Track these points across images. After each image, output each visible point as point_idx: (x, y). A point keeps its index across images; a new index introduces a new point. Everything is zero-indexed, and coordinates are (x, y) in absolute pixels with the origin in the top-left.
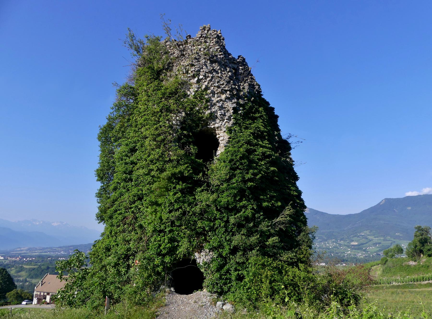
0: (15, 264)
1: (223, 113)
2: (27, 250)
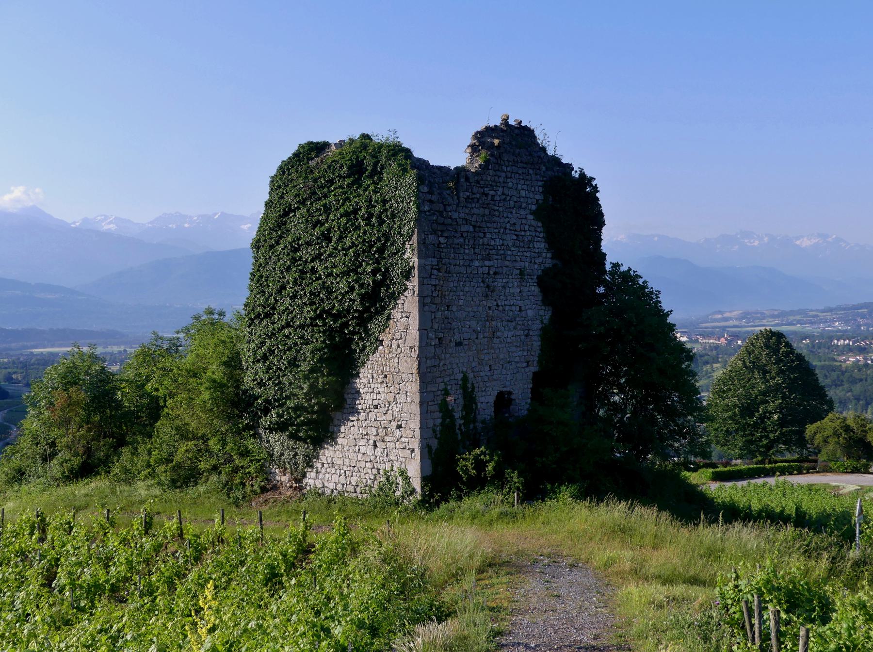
2: (740, 318)
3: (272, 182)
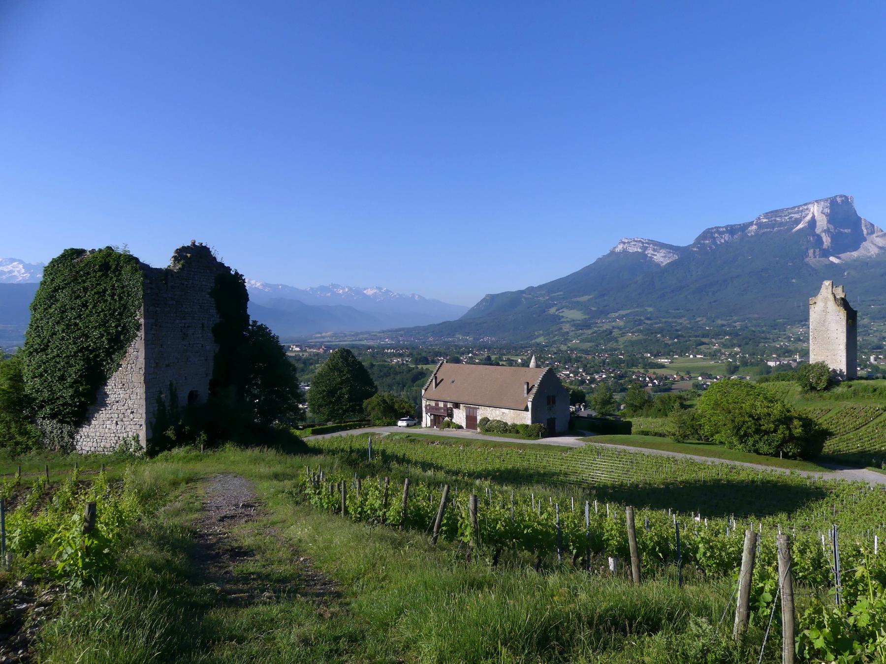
2: (331, 337)
3: (45, 270)
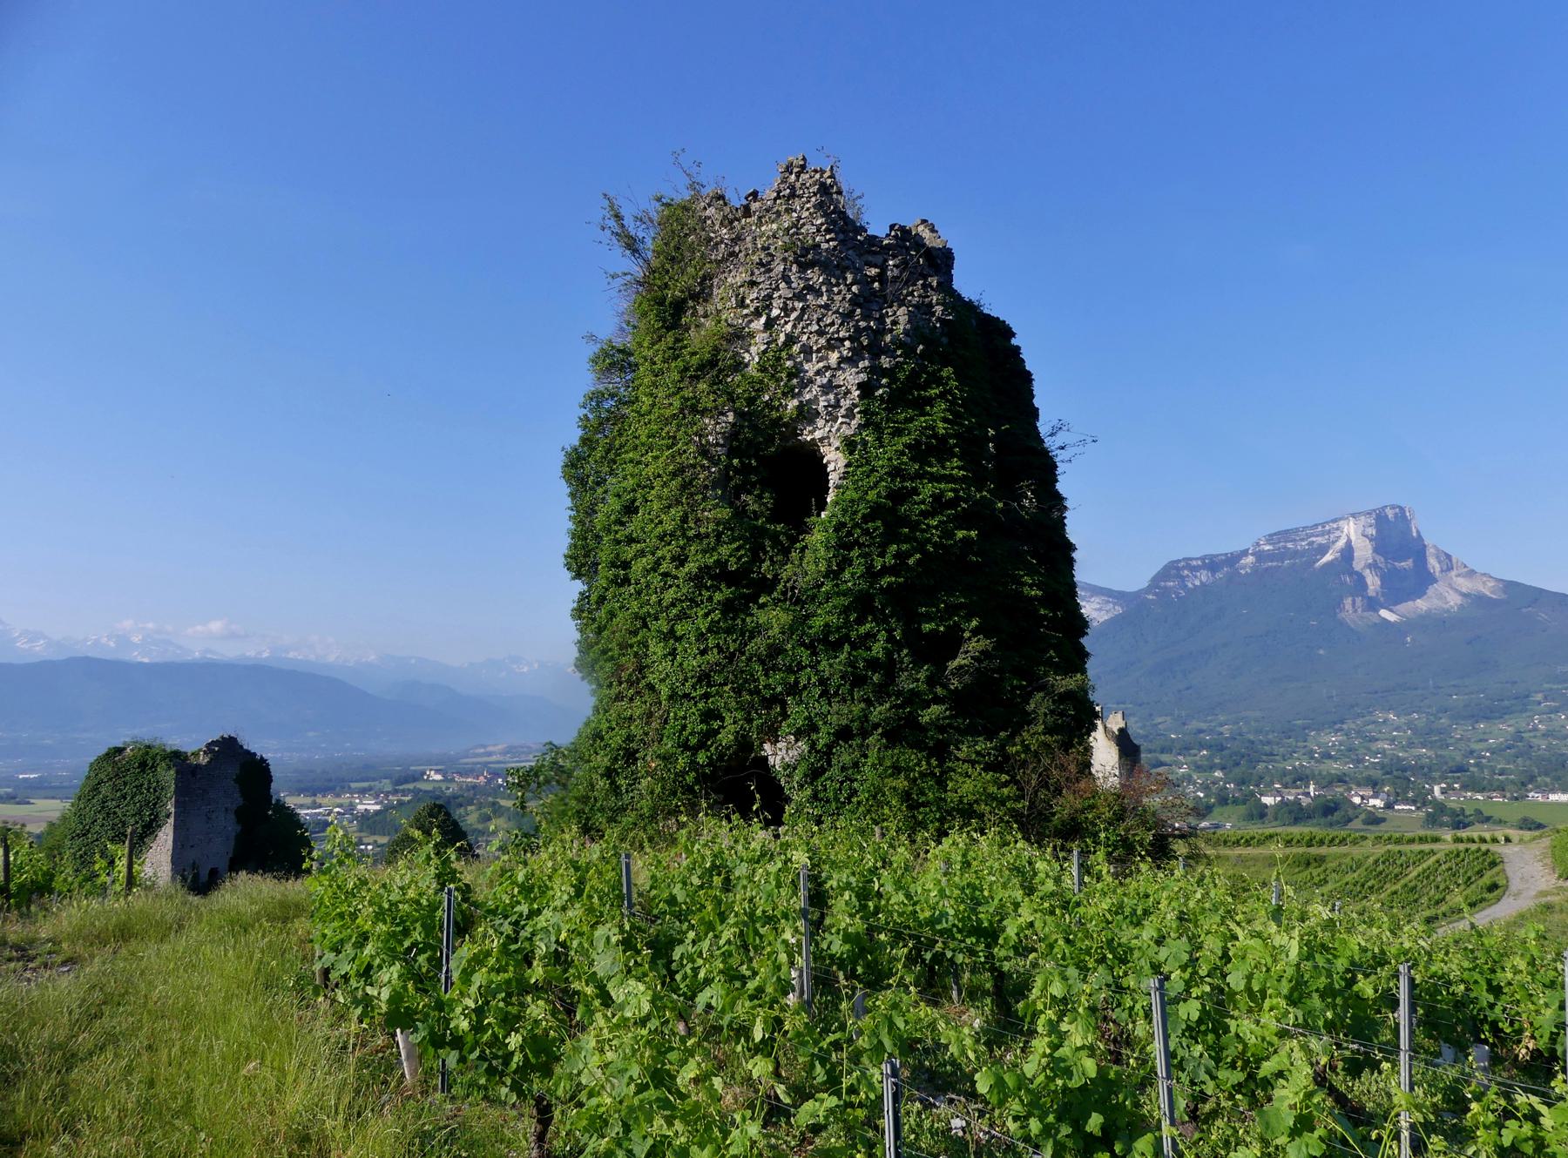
0: (475, 795)
1: (832, 402)
2: (504, 753)
